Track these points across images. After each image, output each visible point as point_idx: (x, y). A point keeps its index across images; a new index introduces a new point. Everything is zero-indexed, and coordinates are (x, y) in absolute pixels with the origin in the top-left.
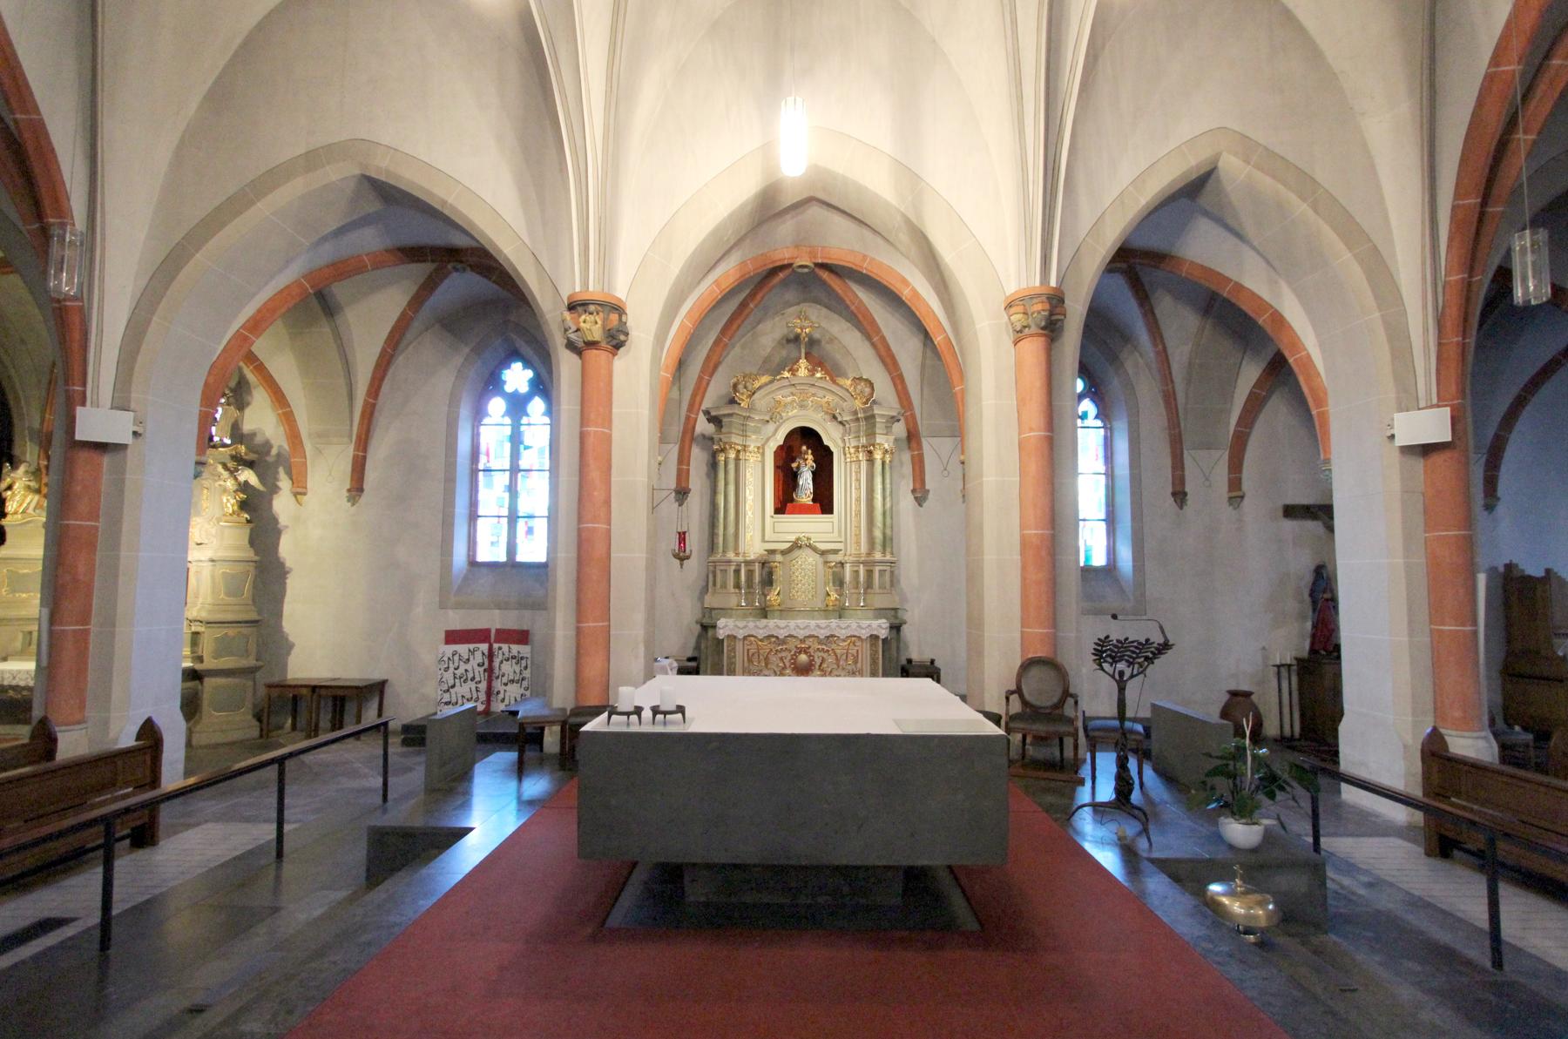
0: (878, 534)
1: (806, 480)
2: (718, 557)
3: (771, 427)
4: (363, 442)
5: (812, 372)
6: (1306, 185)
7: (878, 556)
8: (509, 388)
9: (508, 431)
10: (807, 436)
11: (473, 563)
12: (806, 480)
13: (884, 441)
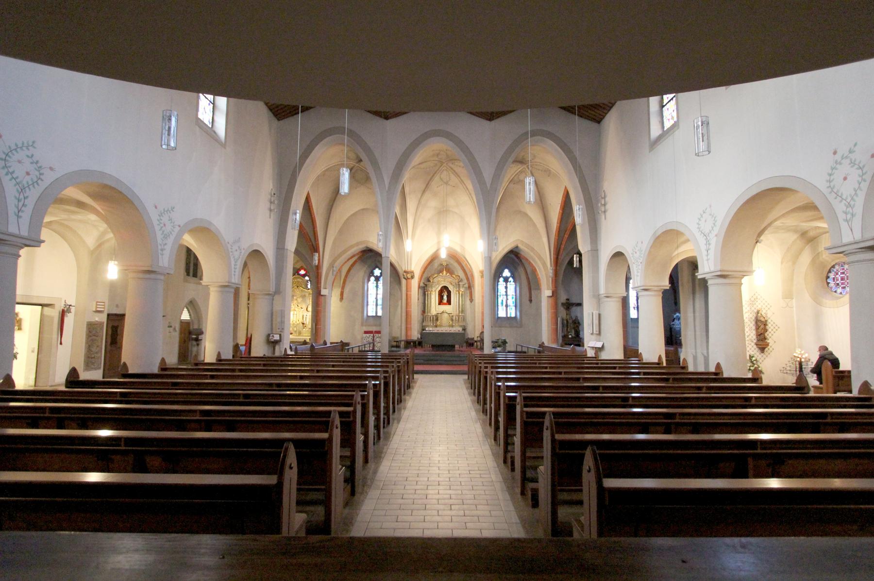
0: (461, 309)
1: (445, 297)
2: (426, 314)
3: (437, 286)
4: (343, 288)
5: (447, 274)
6: (533, 249)
7: (461, 314)
8: (375, 275)
9: (375, 285)
10: (445, 288)
11: (367, 316)
12: (445, 297)
13: (462, 290)
